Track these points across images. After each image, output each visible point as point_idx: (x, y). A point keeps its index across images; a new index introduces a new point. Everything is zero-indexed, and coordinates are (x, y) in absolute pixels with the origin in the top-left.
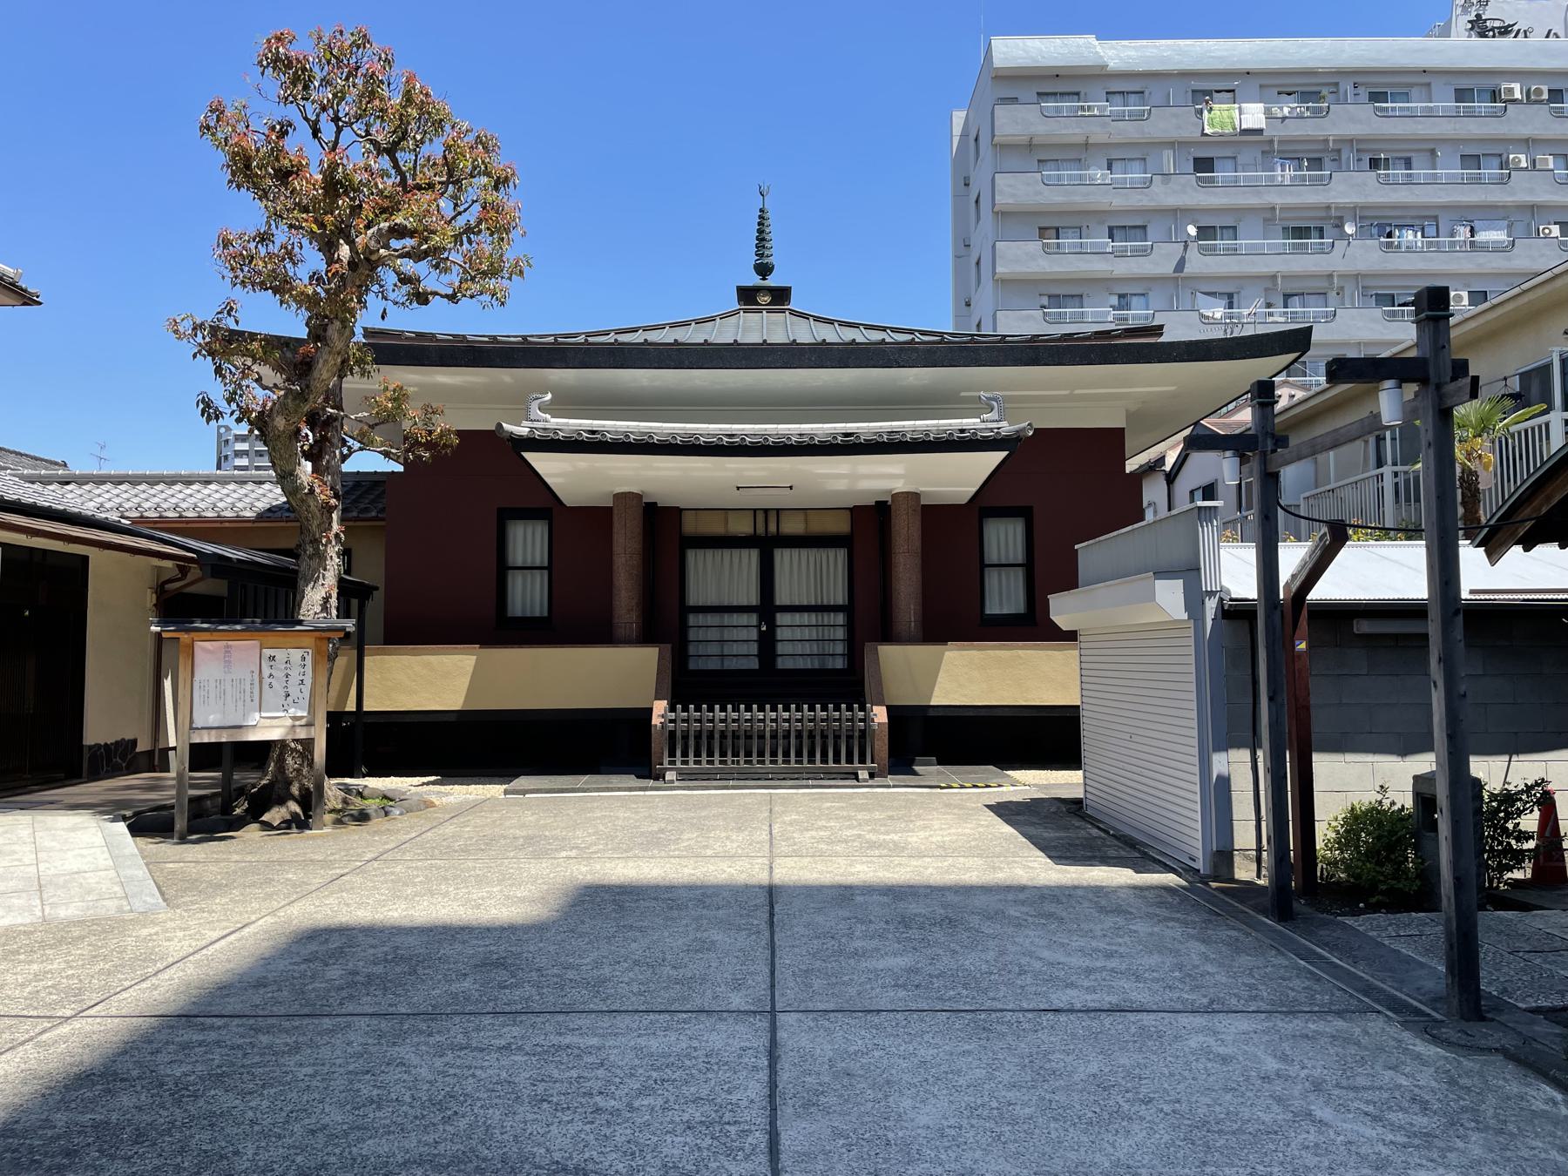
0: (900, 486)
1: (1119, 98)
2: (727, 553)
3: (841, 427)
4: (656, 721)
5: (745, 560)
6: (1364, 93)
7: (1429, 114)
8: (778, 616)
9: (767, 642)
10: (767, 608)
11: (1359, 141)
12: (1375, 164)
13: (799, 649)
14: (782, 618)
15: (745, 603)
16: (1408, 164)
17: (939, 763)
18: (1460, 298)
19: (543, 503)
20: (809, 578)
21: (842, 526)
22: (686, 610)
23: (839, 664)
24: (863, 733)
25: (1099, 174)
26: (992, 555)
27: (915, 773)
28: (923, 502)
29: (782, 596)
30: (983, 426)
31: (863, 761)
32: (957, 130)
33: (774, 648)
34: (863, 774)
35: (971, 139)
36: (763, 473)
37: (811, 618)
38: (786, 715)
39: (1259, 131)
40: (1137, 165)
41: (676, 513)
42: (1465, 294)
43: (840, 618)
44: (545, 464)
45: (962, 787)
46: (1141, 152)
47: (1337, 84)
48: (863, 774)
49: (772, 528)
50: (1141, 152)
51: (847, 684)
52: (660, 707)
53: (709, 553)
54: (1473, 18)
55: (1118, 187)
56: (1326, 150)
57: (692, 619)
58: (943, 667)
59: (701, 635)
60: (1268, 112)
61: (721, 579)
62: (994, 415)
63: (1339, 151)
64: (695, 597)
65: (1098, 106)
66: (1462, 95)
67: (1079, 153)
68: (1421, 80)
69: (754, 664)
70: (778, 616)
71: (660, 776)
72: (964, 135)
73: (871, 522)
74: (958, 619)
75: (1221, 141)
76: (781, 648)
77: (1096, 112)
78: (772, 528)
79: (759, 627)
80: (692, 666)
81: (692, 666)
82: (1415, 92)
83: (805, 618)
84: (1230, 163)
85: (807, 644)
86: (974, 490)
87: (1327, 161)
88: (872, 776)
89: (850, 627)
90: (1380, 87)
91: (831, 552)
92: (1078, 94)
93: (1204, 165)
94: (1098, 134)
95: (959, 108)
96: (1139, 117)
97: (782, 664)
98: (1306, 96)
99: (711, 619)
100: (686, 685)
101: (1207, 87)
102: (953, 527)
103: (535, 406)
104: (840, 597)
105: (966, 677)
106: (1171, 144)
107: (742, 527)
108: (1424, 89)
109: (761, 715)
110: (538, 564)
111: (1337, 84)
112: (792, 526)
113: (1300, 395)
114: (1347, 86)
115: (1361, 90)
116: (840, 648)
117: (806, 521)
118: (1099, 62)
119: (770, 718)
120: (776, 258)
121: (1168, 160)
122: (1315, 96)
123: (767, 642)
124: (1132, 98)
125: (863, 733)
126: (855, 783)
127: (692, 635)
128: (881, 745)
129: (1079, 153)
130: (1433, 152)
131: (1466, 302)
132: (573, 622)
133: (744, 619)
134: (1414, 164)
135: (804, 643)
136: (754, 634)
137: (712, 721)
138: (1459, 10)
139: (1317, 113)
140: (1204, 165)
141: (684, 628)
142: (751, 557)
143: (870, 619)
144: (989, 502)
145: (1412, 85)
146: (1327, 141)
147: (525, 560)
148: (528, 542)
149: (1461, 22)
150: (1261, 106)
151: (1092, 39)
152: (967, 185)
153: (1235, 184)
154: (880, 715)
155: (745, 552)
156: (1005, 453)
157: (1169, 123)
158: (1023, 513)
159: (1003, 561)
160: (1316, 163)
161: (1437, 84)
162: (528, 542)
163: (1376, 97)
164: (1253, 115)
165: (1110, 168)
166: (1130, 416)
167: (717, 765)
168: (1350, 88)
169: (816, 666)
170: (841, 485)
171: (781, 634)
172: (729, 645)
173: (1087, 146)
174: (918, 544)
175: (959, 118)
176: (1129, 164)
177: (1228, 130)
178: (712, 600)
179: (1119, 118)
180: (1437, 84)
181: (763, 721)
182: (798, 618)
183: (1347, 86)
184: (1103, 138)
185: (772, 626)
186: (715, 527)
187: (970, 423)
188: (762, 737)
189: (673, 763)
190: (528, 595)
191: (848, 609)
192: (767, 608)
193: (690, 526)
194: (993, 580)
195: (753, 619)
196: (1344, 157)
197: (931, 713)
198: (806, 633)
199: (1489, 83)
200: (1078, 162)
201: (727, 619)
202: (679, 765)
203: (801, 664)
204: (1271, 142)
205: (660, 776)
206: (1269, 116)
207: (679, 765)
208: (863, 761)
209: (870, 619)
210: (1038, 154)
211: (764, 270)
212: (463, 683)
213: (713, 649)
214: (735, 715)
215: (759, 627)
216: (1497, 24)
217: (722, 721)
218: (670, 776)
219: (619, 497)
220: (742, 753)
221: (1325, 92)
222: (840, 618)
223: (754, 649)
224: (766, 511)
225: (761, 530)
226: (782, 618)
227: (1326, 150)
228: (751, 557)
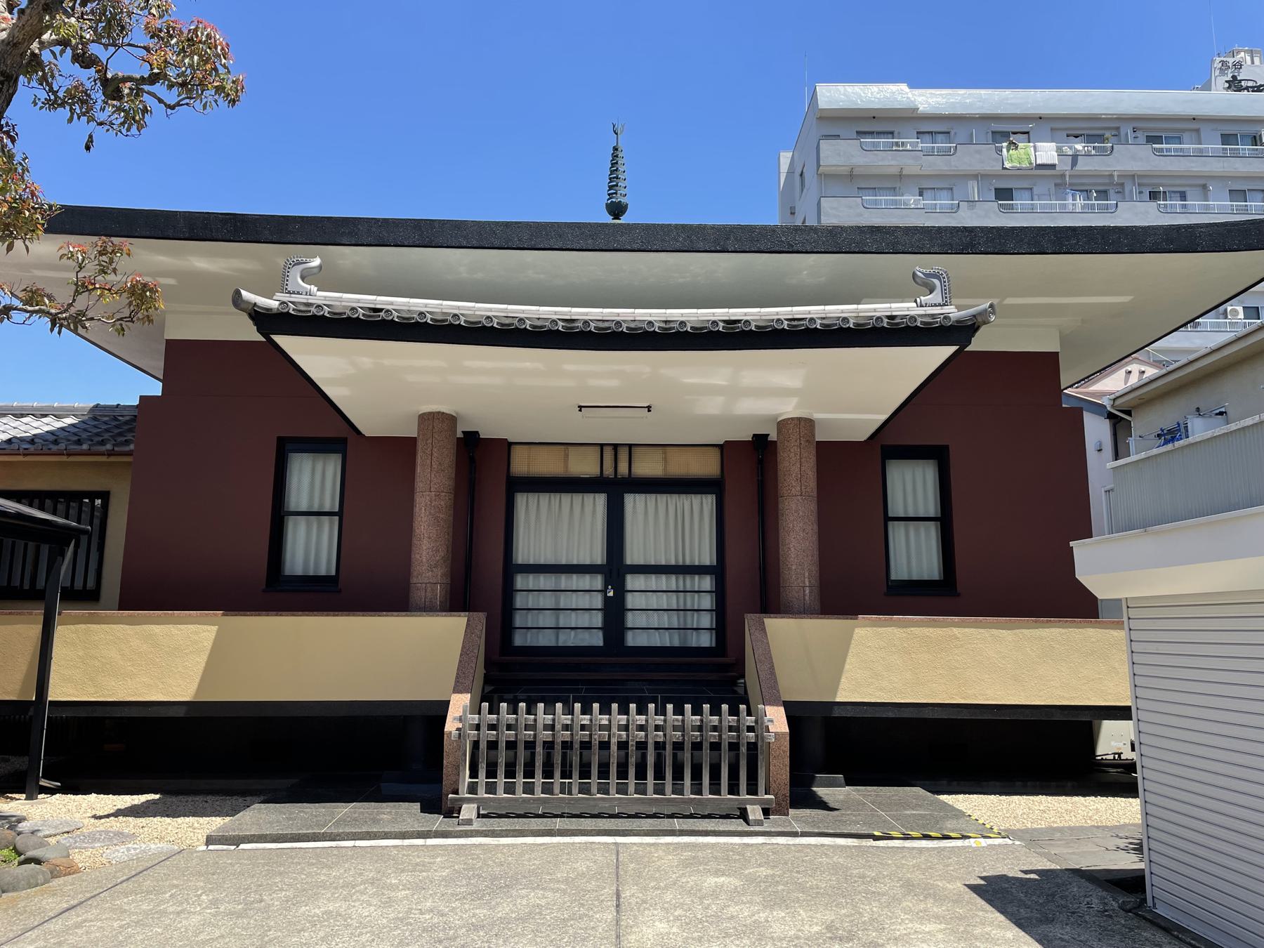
0: (789, 409)
1: (928, 137)
2: (566, 498)
3: (721, 313)
4: (451, 726)
5: (589, 508)
6: (1142, 137)
7: (1200, 154)
8: (629, 578)
9: (615, 611)
10: (614, 568)
11: (1140, 176)
12: (1154, 196)
13: (655, 620)
14: (633, 582)
15: (588, 562)
16: (1183, 196)
17: (849, 782)
18: (1236, 312)
19: (330, 431)
20: (669, 531)
21: (708, 466)
22: (511, 569)
23: (706, 640)
24: (753, 747)
25: (912, 199)
26: (897, 506)
27: (822, 805)
28: (820, 437)
29: (633, 555)
30: (921, 311)
31: (752, 790)
32: (784, 167)
33: (622, 620)
34: (755, 812)
35: (798, 176)
36: (614, 383)
37: (671, 582)
38: (641, 719)
39: (1053, 166)
40: (945, 193)
41: (505, 447)
42: (1240, 309)
43: (707, 583)
44: (315, 357)
45: (907, 837)
46: (948, 183)
47: (1118, 129)
48: (755, 812)
49: (623, 469)
50: (948, 183)
51: (715, 673)
52: (459, 704)
53: (544, 498)
54: (1229, 78)
55: (932, 211)
56: (1111, 184)
57: (520, 581)
58: (853, 650)
59: (531, 600)
60: (1059, 150)
61: (556, 531)
62: (936, 297)
63: (1122, 184)
64: (525, 552)
65: (910, 142)
66: (1227, 139)
67: (894, 182)
68: (1193, 125)
69: (597, 640)
70: (629, 578)
71: (451, 812)
72: (790, 172)
73: (745, 470)
74: (860, 587)
75: (1019, 174)
76: (631, 620)
77: (909, 147)
78: (623, 469)
79: (604, 591)
80: (519, 640)
81: (519, 640)
82: (1186, 136)
83: (663, 582)
84: (1027, 194)
85: (665, 615)
86: (884, 417)
87: (1112, 192)
88: (766, 812)
89: (720, 593)
90: (1156, 131)
91: (696, 499)
92: (892, 133)
93: (1004, 194)
94: (912, 165)
95: (786, 150)
96: (946, 153)
97: (633, 640)
98: (1090, 138)
99: (544, 581)
100: (510, 671)
101: (1006, 130)
102: (850, 467)
103: (295, 274)
104: (705, 554)
105: (890, 664)
106: (975, 177)
107: (585, 466)
108: (1194, 135)
109: (604, 720)
110: (327, 508)
111: (1118, 129)
112: (647, 467)
113: (1151, 372)
114: (1127, 130)
115: (1139, 134)
116: (706, 620)
117: (665, 460)
118: (912, 106)
119: (612, 723)
120: (626, 196)
121: (973, 189)
122: (1101, 138)
123: (615, 611)
124: (940, 137)
125: (753, 747)
126: (738, 825)
127: (519, 601)
128: (778, 767)
129: (894, 182)
130: (1204, 187)
131: (1241, 315)
132: (368, 584)
133: (586, 581)
134: (1188, 197)
135: (663, 615)
136: (598, 601)
137: (533, 727)
138: (1217, 72)
139: (1102, 152)
140: (1004, 194)
141: (509, 591)
142: (597, 504)
143: (747, 583)
144: (891, 443)
145: (1184, 130)
146: (1111, 176)
147: (321, 505)
148: (313, 481)
149: (1220, 82)
150: (1054, 144)
151: (904, 87)
152: (793, 214)
153: (1032, 210)
154: (776, 720)
155: (589, 498)
156: (954, 348)
157: (974, 157)
158: (938, 454)
159: (911, 515)
160: (1103, 194)
161: (1206, 131)
162: (313, 481)
163: (1152, 139)
164: (1047, 152)
165: (921, 194)
166: (1064, 339)
167: (539, 794)
168: (1130, 132)
169: (676, 643)
170: (712, 406)
171: (631, 601)
172: (561, 615)
173: (900, 176)
174: (812, 484)
175: (785, 158)
176: (938, 193)
177: (1025, 164)
178: (545, 556)
179: (930, 153)
180: (1206, 131)
181: (608, 728)
182: (653, 582)
183: (1127, 130)
184: (914, 170)
185: (621, 591)
186: (546, 465)
187: (904, 308)
188: (605, 745)
189: (473, 789)
190: (310, 548)
191: (718, 571)
192: (614, 568)
193: (522, 464)
194: (899, 536)
195: (597, 582)
196: (1127, 190)
197: (837, 713)
198: (664, 601)
199: (1251, 129)
200: (893, 191)
201: (565, 581)
202: (482, 794)
203: (656, 640)
204: (1063, 176)
205: (451, 812)
206: (1061, 154)
207: (482, 794)
208: (752, 790)
209: (747, 583)
210: (855, 181)
211: (617, 210)
212: (196, 664)
213: (546, 620)
214: (566, 719)
215: (604, 591)
216: (1250, 84)
217: (546, 727)
218: (468, 811)
219: (427, 419)
220: (576, 774)
221: (1108, 134)
222: (707, 583)
223: (597, 620)
224: (616, 447)
225: (609, 471)
226: (633, 582)
227: (1111, 184)
228: (597, 504)
